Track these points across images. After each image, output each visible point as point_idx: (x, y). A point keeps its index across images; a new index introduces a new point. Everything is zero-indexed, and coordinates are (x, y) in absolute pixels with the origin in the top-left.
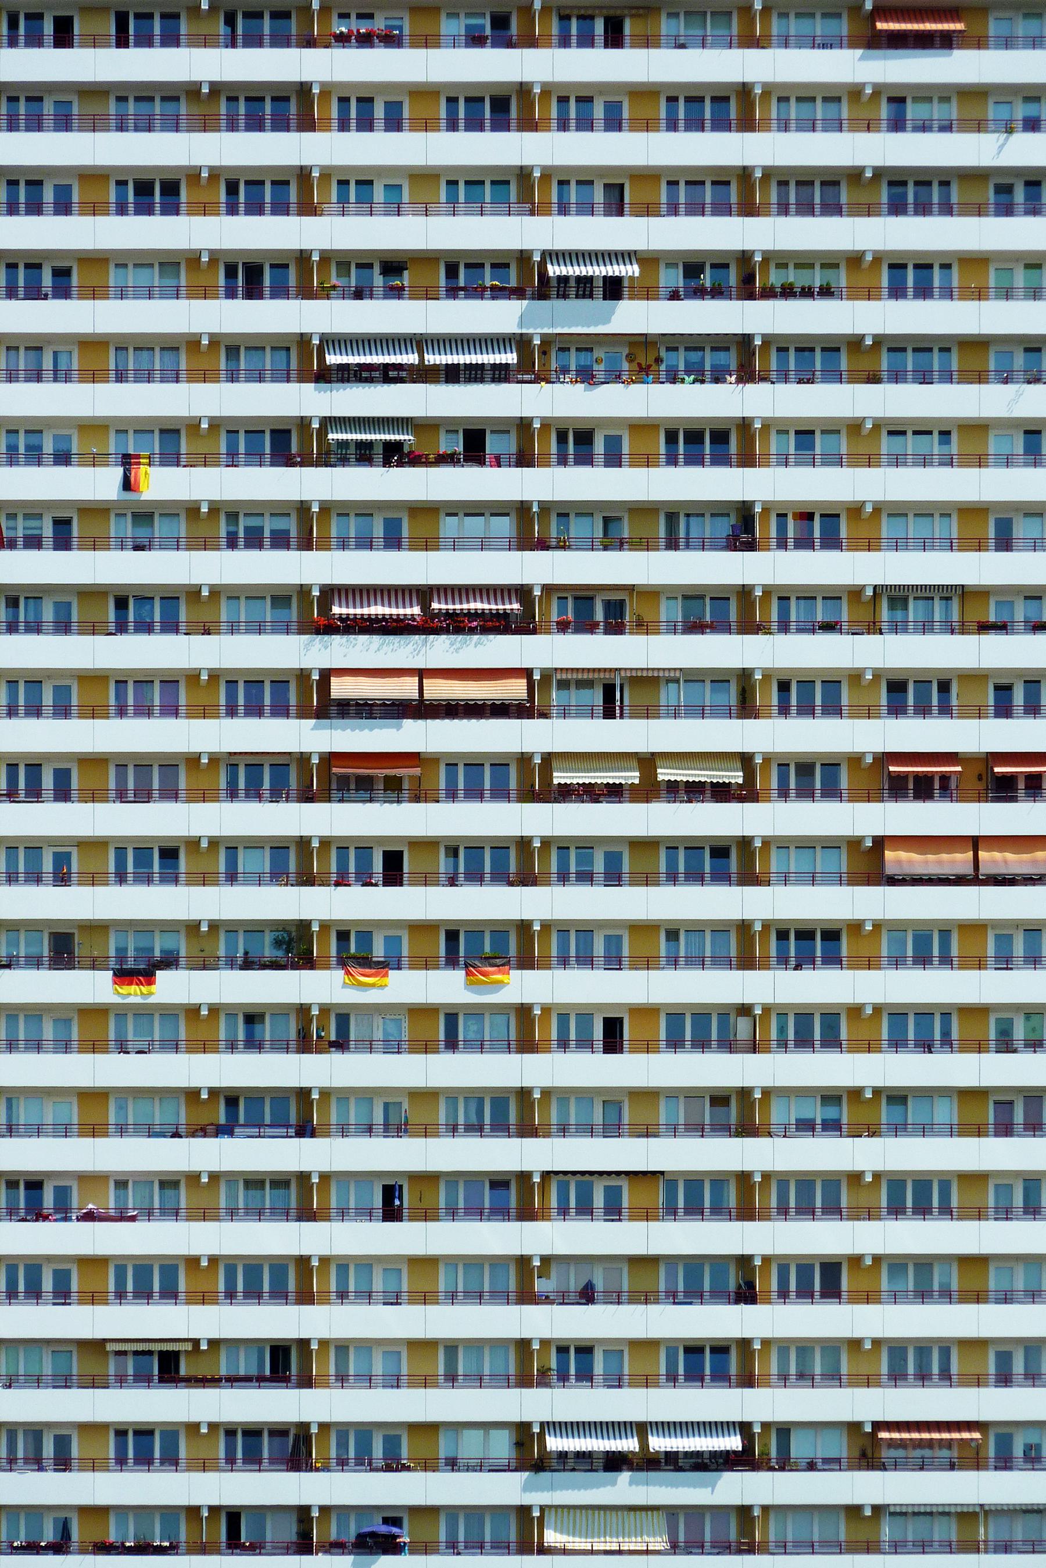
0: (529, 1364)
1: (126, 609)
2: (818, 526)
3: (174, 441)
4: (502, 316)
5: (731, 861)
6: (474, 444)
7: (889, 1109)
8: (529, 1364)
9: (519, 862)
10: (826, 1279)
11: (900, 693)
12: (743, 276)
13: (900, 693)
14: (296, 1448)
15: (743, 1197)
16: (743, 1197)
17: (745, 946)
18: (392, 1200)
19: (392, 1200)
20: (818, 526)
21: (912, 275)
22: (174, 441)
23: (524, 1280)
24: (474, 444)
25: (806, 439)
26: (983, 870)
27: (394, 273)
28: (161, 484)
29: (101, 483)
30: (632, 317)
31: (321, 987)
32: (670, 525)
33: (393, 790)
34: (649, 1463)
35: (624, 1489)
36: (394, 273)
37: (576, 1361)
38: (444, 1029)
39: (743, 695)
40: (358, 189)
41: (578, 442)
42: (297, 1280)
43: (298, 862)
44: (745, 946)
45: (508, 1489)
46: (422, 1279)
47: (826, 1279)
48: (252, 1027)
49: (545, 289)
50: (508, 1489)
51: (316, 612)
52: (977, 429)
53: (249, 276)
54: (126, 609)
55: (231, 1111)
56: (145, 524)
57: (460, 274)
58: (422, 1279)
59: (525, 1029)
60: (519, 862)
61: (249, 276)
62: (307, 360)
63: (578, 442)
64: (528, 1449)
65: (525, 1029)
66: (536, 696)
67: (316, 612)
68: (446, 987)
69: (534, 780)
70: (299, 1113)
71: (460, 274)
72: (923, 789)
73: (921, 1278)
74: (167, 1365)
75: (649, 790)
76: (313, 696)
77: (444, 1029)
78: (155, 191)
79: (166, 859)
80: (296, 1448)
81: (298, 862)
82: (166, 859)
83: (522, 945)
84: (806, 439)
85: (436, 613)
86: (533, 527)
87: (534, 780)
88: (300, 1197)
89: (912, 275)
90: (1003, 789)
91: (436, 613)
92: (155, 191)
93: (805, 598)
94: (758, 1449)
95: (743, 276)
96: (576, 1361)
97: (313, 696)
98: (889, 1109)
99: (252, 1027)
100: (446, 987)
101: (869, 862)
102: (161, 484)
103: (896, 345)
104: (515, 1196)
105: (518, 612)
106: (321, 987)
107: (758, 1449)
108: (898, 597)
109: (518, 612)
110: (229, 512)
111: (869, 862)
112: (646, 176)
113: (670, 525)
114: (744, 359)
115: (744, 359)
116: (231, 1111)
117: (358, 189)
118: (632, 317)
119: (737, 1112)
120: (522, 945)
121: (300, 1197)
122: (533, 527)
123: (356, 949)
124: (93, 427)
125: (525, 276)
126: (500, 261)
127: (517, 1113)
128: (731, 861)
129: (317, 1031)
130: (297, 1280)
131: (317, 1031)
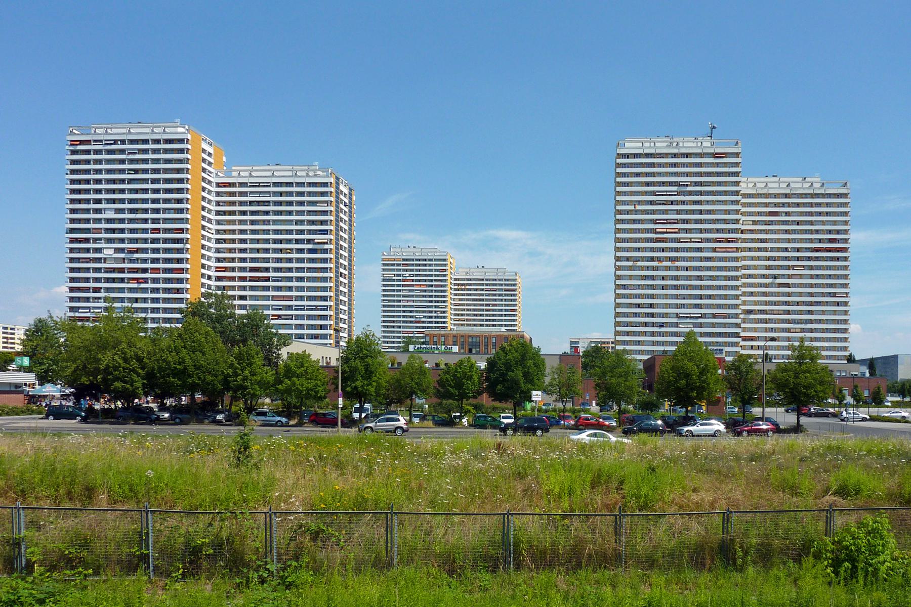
0: (678, 306)
1: (635, 221)
2: (709, 212)
3: (640, 203)
4: (675, 188)
5: (699, 250)
6: (672, 203)
7: (717, 278)
8: (678, 306)
9: (677, 250)
10: (710, 297)
11: (718, 231)
12: (700, 184)
13: (718, 231)
14: (652, 315)
15: (701, 287)
16: (701, 287)
17: (701, 259)
18: (663, 287)
19: (663, 287)
20: (709, 212)
21: (719, 184)
22: (640, 203)
23: (677, 297)
24: (672, 203)
25: (708, 202)
26: (766, 416)
27: (663, 184)
28: (638, 207)
29: (632, 207)
30: (689, 189)
31: (655, 264)
32: (693, 212)
33: (663, 242)
34: (691, 317)
35: (688, 320)
36: (663, 184)
37: (683, 306)
38: (668, 268)
39: (701, 231)
40: (659, 174)
41: (683, 203)
42: (652, 296)
43: (653, 250)
44: (701, 259)
45: (675, 320)
46: (666, 296)
47: (710, 297)
48: (648, 268)
49: (680, 185)
50: (675, 320)
51: (654, 222)
52: (726, 201)
53: (648, 184)
54: (635, 221)
55: (646, 278)
56: (636, 212)
57: (671, 184)
58: (666, 296)
59: (677, 269)
60: (677, 250)
61: (648, 184)
62: (654, 193)
63: (683, 203)
64: (677, 316)
65: (677, 269)
66: (680, 231)
67: (654, 222)
68: (669, 264)
69: (678, 240)
70: (653, 278)
71: (671, 184)
72: (720, 242)
73: (720, 297)
74: (639, 306)
75: (691, 242)
76: (654, 231)
77: (668, 268)
78: (638, 175)
79: (638, 250)
80: (652, 315)
81: (653, 250)
82: (638, 250)
83: (676, 259)
84: (708, 202)
85: (668, 222)
86: (678, 212)
87: (678, 240)
88: (653, 287)
89: (719, 184)
90: (729, 242)
91: (668, 222)
92: (638, 175)
93: (744, 387)
94: (703, 316)
95: (700, 184)
96: (683, 306)
97: (654, 231)
98: (717, 278)
99: (648, 268)
100: (669, 264)
101: (714, 250)
102: (638, 207)
103: (717, 192)
104: (676, 287)
105: (677, 222)
106: (655, 264)
107: (703, 316)
108: (718, 220)
109: (677, 222)
110: (645, 211)
111: (714, 250)
112: (691, 173)
113: (693, 212)
114: (701, 193)
115: (701, 193)
116: (646, 278)
117: (659, 174)
118: (689, 189)
119: (700, 278)
120: (676, 259)
121: (653, 287)
122: (678, 212)
123: (659, 259)
124: (631, 201)
125: (677, 184)
126: (675, 182)
127: (676, 278)
128: (699, 250)
129: (654, 269)
130: (652, 296)
131: (654, 269)
